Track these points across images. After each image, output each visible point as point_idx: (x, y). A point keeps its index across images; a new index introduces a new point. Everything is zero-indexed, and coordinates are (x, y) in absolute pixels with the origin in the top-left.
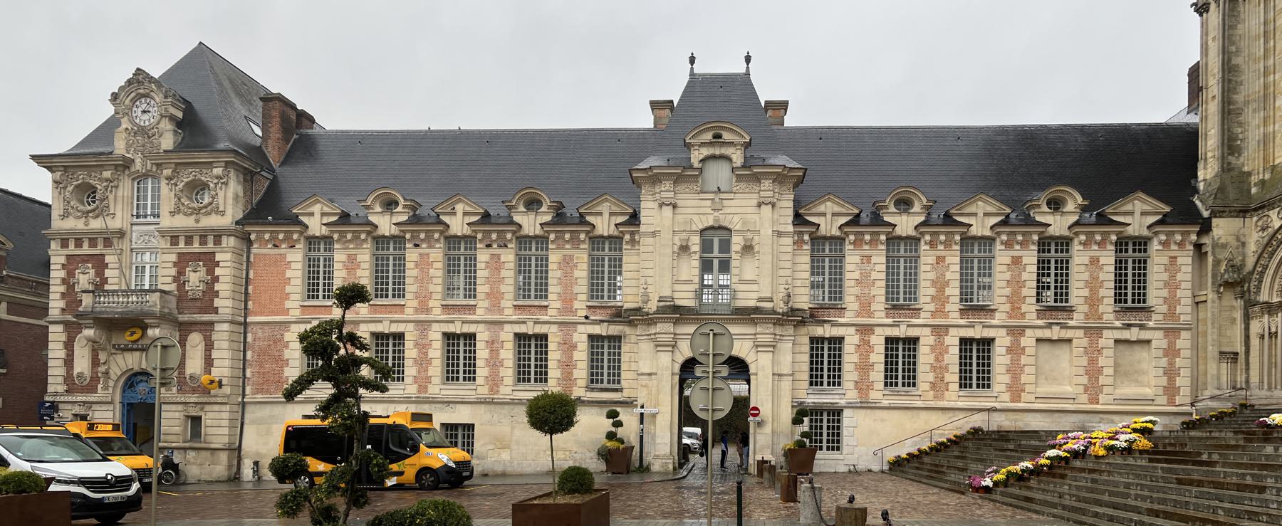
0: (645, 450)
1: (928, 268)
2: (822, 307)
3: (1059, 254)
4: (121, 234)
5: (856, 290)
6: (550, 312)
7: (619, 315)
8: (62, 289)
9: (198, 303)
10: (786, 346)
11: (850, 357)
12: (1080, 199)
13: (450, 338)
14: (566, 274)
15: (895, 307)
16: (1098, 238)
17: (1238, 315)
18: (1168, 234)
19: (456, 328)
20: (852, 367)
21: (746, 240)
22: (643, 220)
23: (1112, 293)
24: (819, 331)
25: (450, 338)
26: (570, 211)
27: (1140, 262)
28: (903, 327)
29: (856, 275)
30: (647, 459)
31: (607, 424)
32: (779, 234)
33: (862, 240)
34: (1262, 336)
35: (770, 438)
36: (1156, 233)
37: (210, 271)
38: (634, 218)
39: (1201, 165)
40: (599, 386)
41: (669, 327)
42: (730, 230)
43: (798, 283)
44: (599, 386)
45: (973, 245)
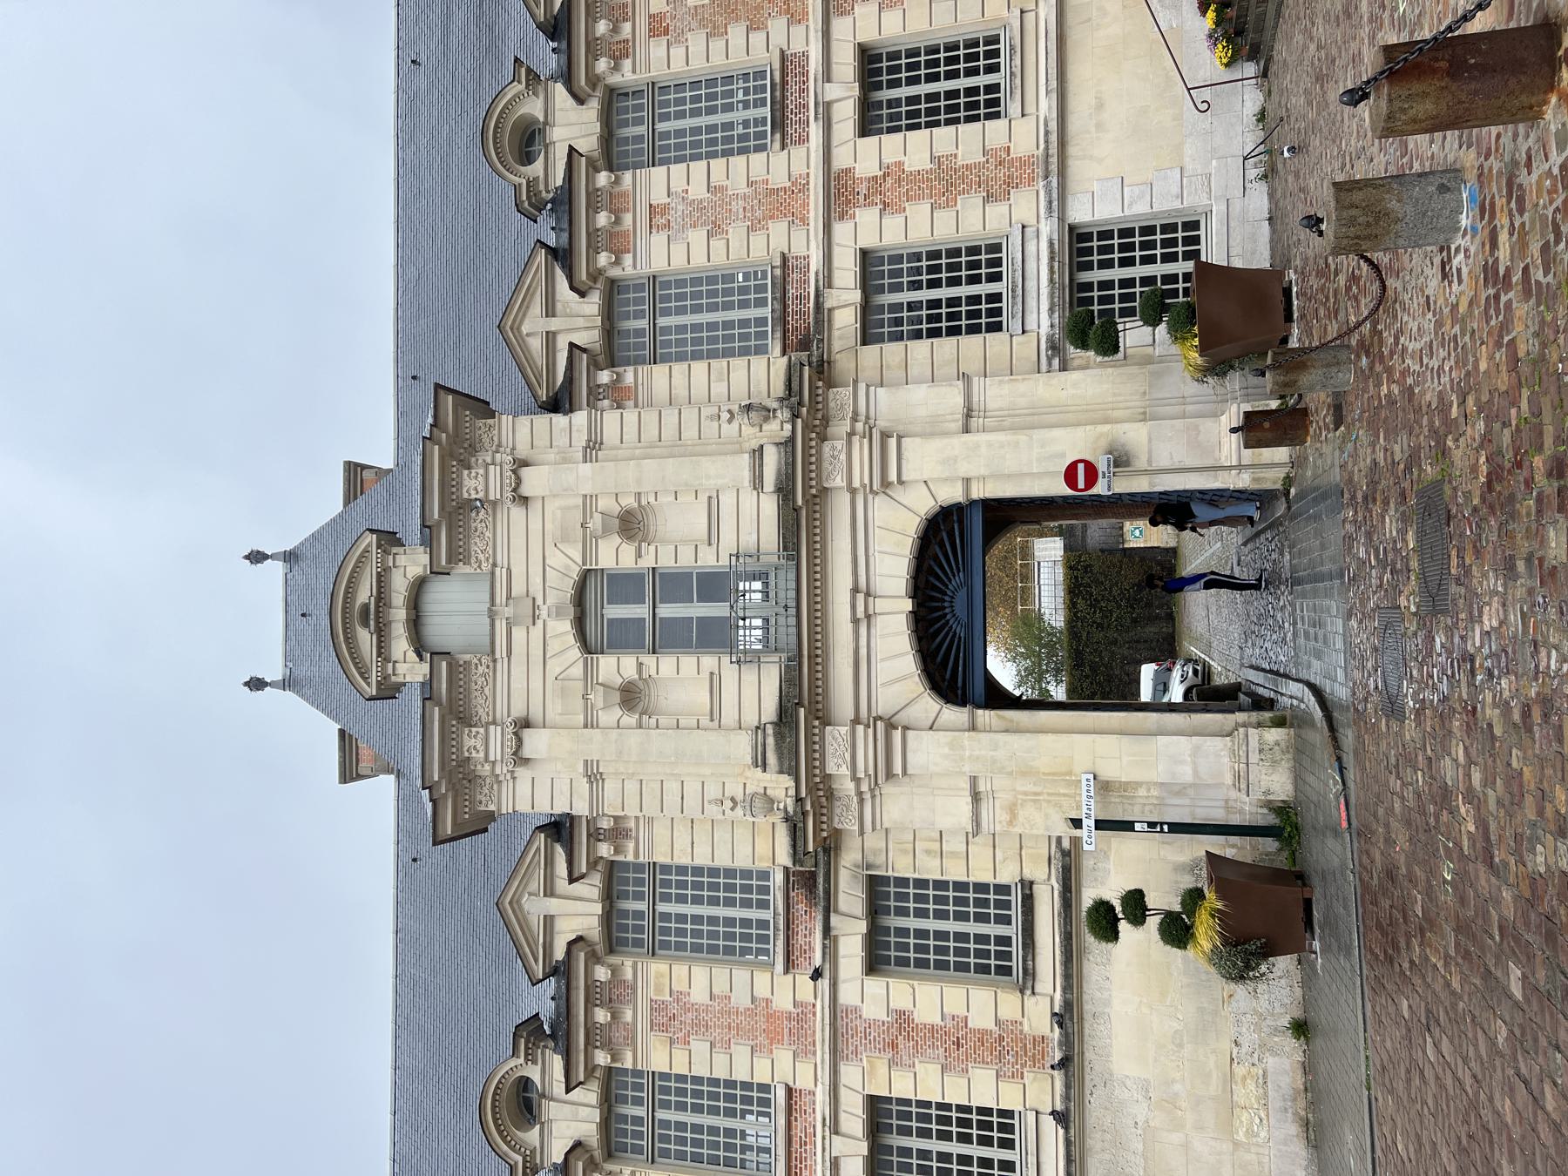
0: (1218, 816)
1: (678, 53)
2: (782, 319)
5: (736, 233)
6: (804, 1081)
7: (811, 876)
10: (887, 404)
11: (918, 227)
14: (701, 1026)
15: (779, 123)
19: (844, 94)
20: (945, 220)
21: (606, 531)
22: (561, 808)
23: (738, 161)
24: (845, 320)
26: (541, 1001)
28: (832, 91)
29: (697, 237)
30: (1248, 811)
31: (1138, 940)
32: (593, 447)
33: (611, 235)
35: (1170, 423)
38: (559, 829)
40: (1016, 949)
41: (836, 737)
42: (585, 575)
43: (719, 389)
44: (1016, 949)
45: (624, 914)
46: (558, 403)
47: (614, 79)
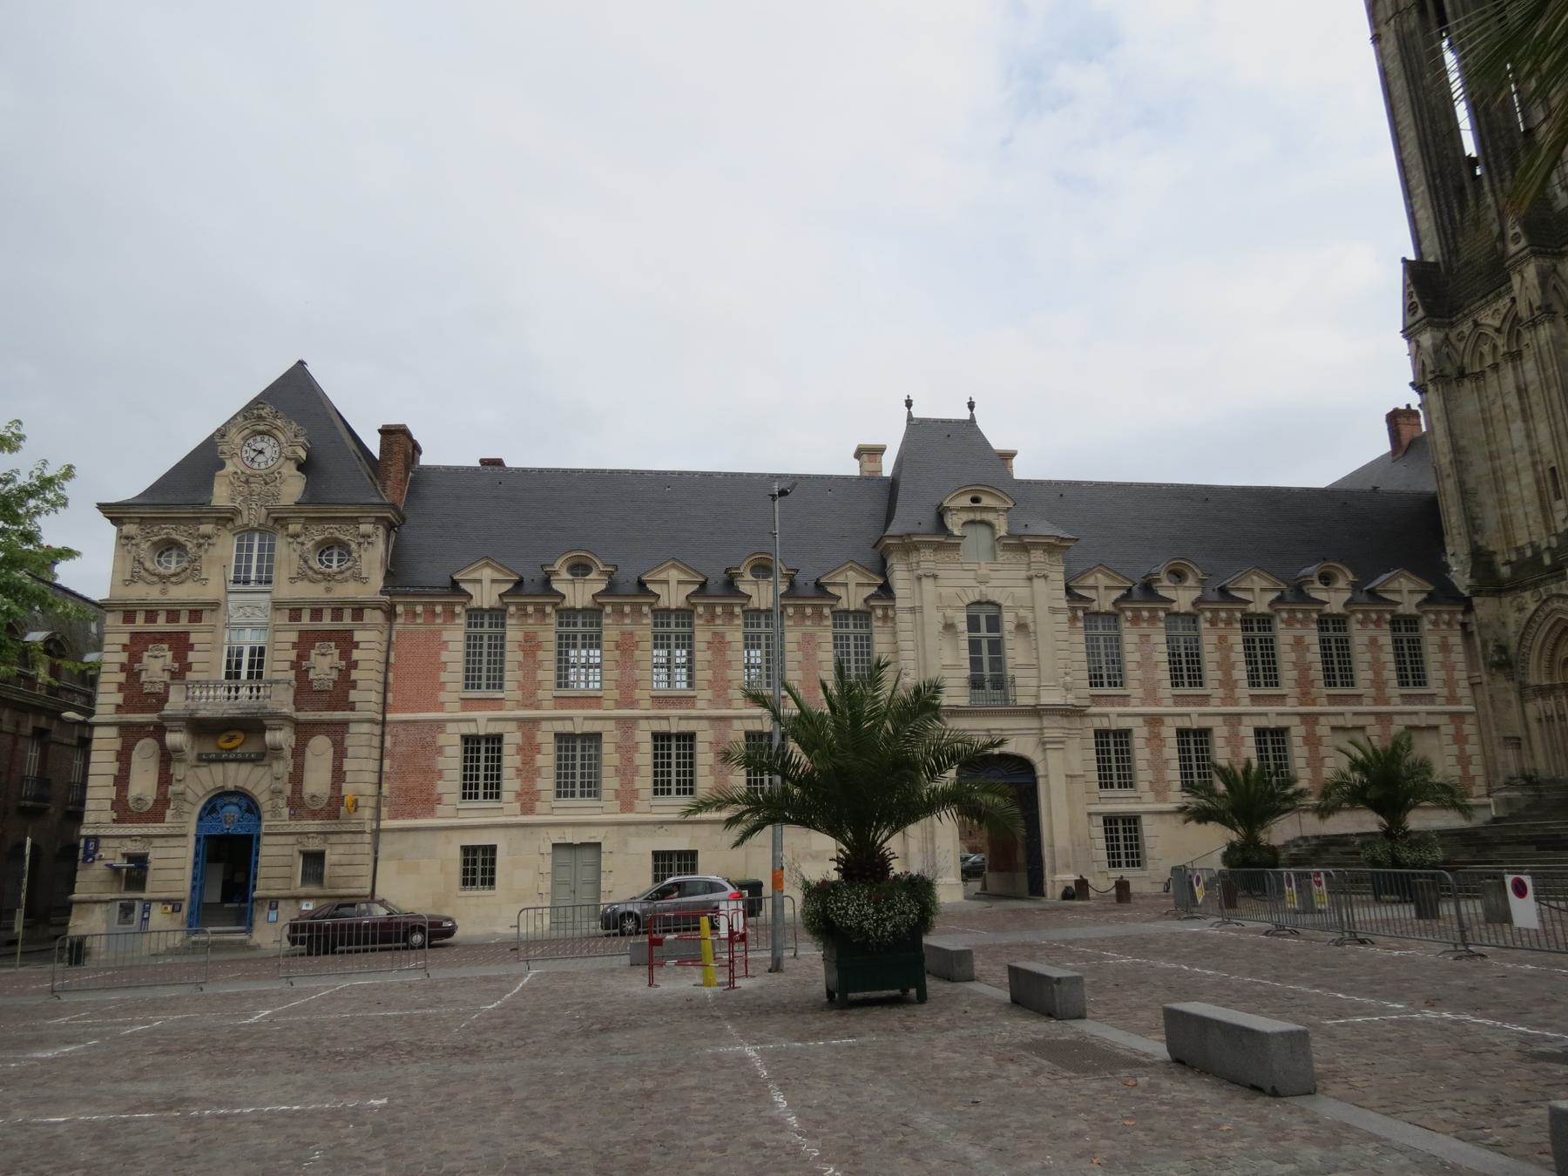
1: (1288, 648)
3: (588, 628)
4: (215, 605)
8: (122, 677)
9: (326, 697)
12: (1351, 577)
13: (471, 742)
14: (807, 657)
16: (1374, 616)
17: (1513, 696)
18: (1438, 613)
23: (1168, 675)
25: (471, 742)
26: (805, 578)
27: (567, 637)
28: (674, 722)
32: (1054, 611)
33: (434, 611)
34: (1540, 720)
36: (1425, 612)
37: (345, 655)
38: (886, 590)
39: (1447, 539)
42: (999, 606)
46: (1068, 590)
47: (1201, 619)
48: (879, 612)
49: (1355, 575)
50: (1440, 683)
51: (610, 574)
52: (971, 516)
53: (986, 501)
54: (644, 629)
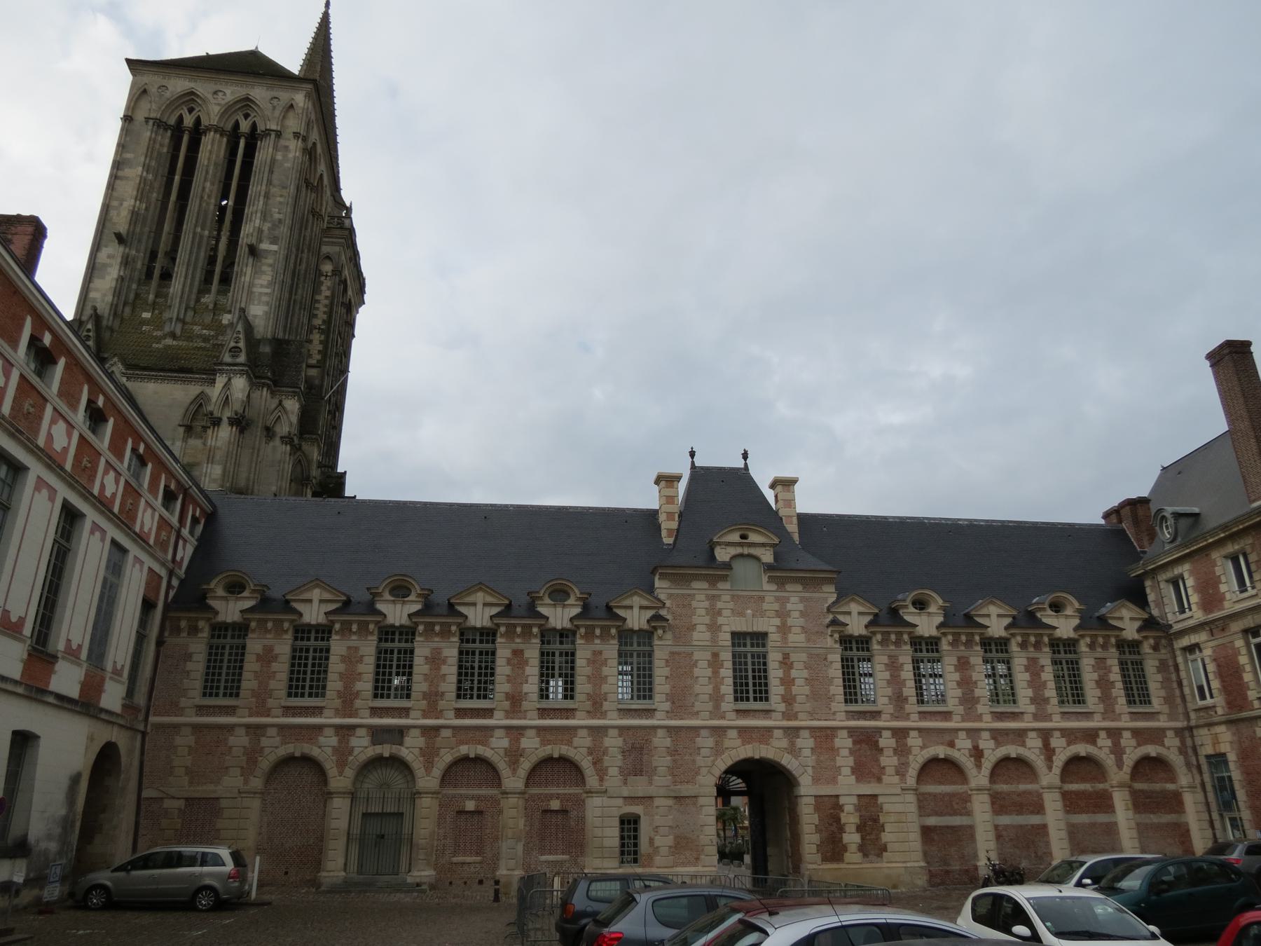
27: (217, 648)
33: (531, 632)
48: (582, 630)
49: (945, 601)
50: (1028, 701)
51: (426, 597)
52: (739, 550)
53: (754, 538)
54: (611, 649)
